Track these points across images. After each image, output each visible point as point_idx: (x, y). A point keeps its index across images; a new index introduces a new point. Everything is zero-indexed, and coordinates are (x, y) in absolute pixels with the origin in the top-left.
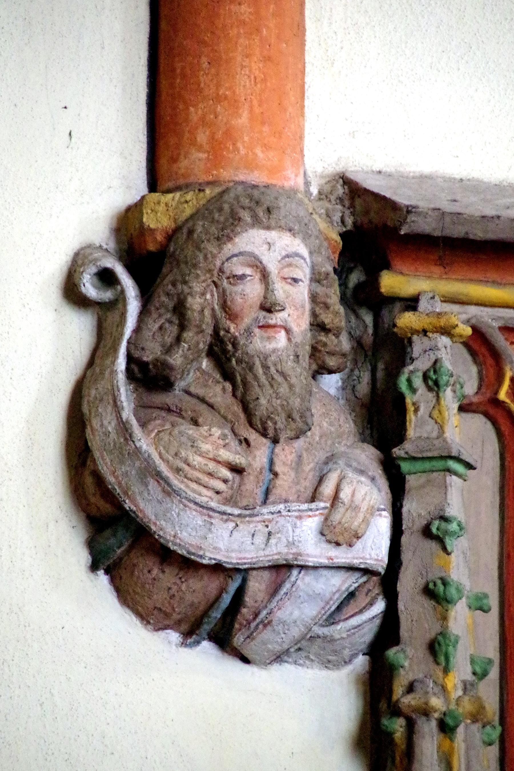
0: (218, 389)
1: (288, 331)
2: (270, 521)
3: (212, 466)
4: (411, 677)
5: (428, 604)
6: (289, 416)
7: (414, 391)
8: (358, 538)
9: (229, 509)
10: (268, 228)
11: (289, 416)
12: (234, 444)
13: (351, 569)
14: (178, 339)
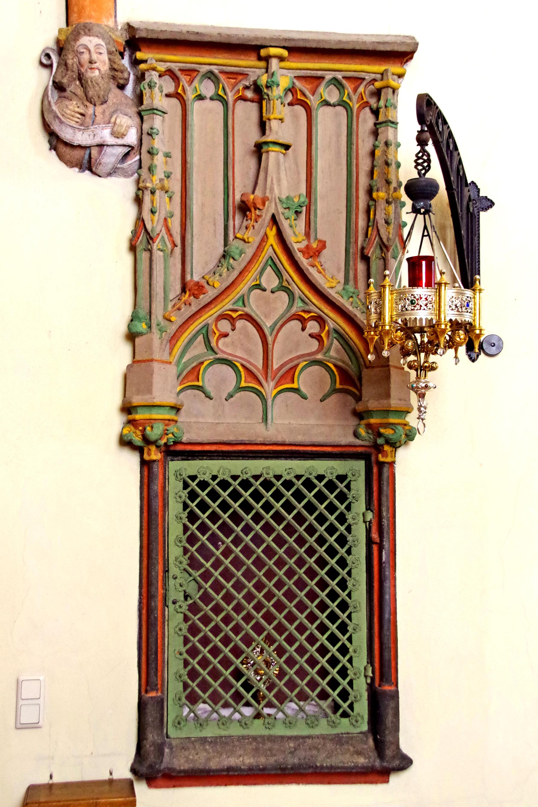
0: (79, 90)
1: (99, 70)
3: (73, 113)
4: (144, 178)
5: (149, 155)
6: (99, 97)
7: (145, 89)
8: (125, 135)
9: (80, 127)
10: (90, 36)
11: (99, 97)
12: (82, 107)
13: (124, 146)
14: (66, 74)
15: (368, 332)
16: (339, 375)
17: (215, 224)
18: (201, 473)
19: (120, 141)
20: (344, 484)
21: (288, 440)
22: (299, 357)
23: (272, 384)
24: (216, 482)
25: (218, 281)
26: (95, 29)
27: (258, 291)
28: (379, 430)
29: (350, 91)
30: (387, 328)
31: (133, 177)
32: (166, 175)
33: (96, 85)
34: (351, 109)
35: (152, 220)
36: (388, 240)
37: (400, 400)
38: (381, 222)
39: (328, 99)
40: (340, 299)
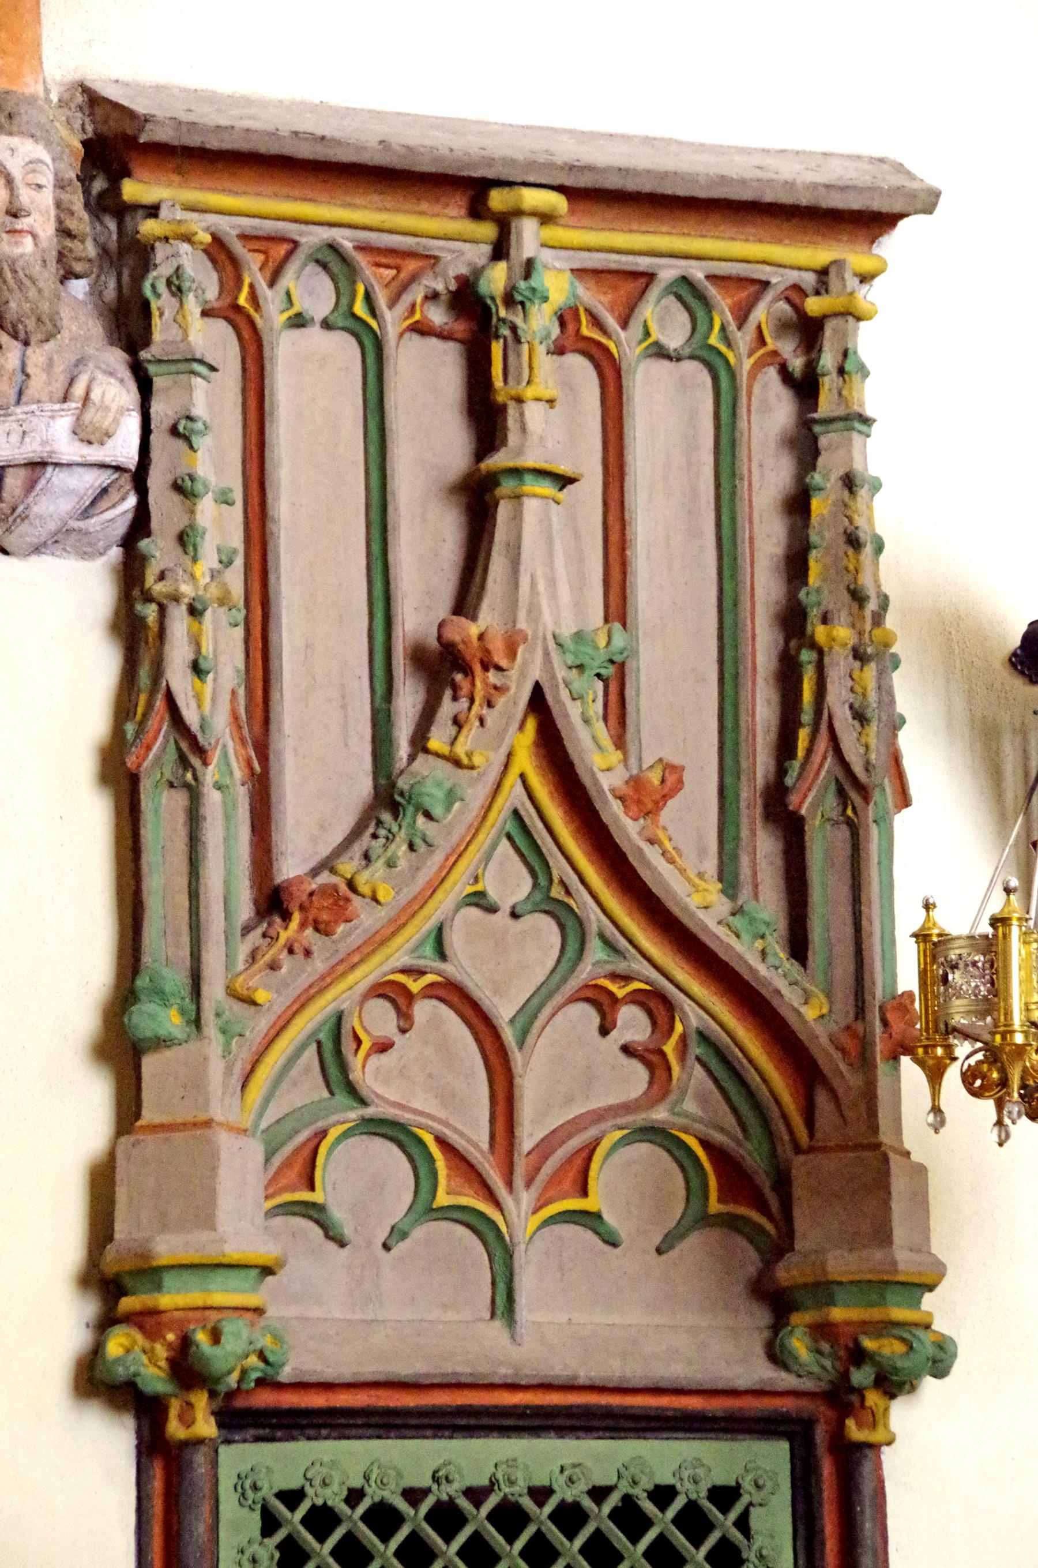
1: (35, 236)
2: (24, 421)
5: (176, 498)
6: (39, 320)
7: (158, 296)
15: (926, 1047)
16: (715, 1171)
17: (344, 707)
18: (317, 1482)
19: (95, 454)
20: (733, 1515)
21: (584, 1374)
22: (598, 1116)
23: (527, 1198)
24: (360, 1510)
25: (385, 880)
26: (26, 115)
27: (474, 912)
28: (856, 1342)
29: (730, 318)
30: (1019, 1039)
31: (104, 559)
32: (224, 559)
33: (28, 283)
34: (733, 375)
35: (198, 697)
36: (867, 770)
37: (911, 1250)
38: (842, 717)
39: (664, 340)
40: (732, 941)
